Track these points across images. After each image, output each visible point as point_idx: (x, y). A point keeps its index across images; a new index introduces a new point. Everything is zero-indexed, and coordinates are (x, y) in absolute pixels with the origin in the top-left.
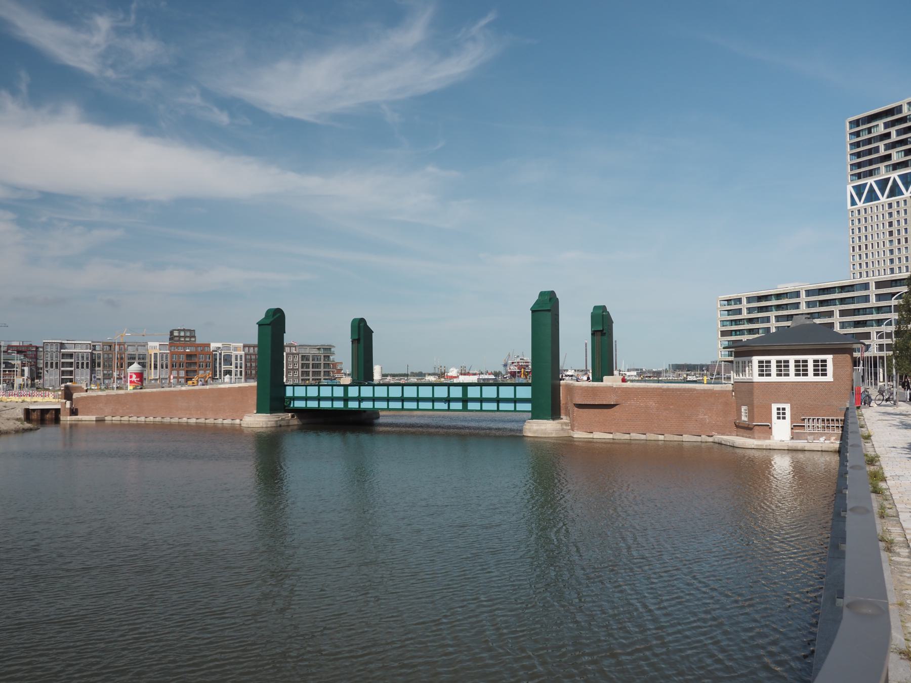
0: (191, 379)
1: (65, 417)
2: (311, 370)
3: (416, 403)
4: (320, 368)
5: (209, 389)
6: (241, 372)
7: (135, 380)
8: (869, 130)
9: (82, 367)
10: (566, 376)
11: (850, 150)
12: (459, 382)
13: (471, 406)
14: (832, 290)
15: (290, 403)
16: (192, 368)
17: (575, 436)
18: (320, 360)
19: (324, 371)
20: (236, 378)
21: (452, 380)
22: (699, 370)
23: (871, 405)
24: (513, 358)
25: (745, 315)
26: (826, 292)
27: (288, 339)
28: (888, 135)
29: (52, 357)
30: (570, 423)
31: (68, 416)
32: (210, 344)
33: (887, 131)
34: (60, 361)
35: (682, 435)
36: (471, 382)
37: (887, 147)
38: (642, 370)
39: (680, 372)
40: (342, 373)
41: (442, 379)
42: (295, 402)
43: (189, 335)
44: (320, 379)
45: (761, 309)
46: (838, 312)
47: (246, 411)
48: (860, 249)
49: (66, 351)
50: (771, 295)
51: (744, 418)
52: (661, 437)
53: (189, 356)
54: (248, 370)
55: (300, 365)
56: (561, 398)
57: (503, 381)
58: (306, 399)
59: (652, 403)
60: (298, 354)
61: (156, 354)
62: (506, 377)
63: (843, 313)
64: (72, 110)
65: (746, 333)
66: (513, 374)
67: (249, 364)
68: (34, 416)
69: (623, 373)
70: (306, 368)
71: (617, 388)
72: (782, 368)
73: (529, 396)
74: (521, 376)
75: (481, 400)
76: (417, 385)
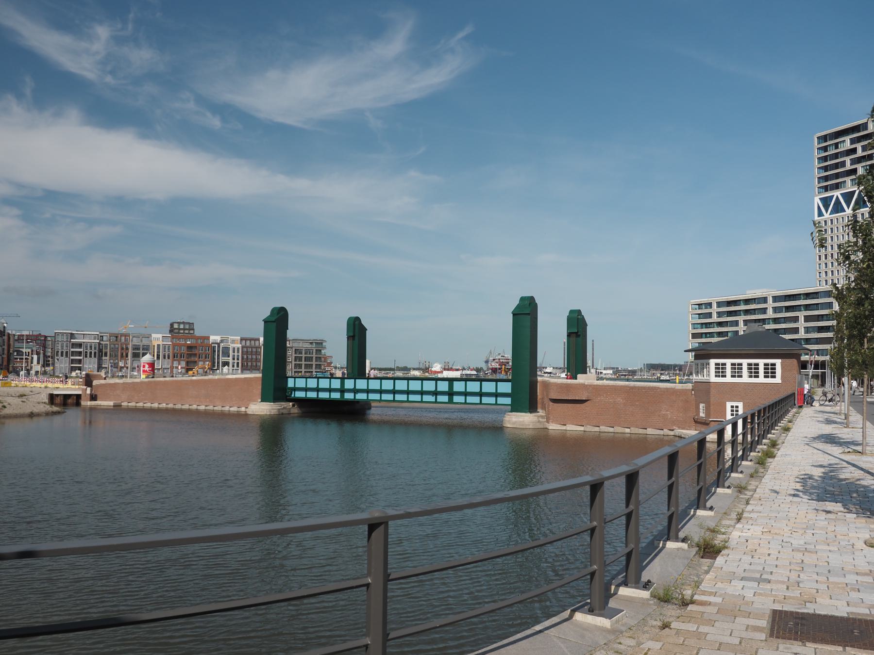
0: (191, 369)
1: (85, 402)
2: (303, 363)
3: (494, 398)
4: (312, 361)
5: (218, 379)
6: (238, 363)
7: (148, 369)
8: (836, 146)
9: (90, 356)
10: (545, 373)
11: (818, 164)
12: (443, 377)
13: (457, 399)
14: (797, 296)
15: (292, 393)
16: (193, 359)
17: (550, 428)
18: (312, 354)
19: (316, 364)
20: (233, 369)
21: (436, 375)
22: (672, 370)
23: (813, 405)
24: (495, 355)
25: (715, 318)
26: (792, 299)
27: (291, 334)
28: (854, 151)
29: (62, 347)
30: (546, 416)
31: (88, 401)
32: (209, 337)
33: (853, 146)
34: (70, 350)
35: (646, 429)
36: (455, 377)
37: (853, 162)
38: (618, 368)
39: (654, 372)
40: (332, 367)
41: (427, 374)
42: (296, 392)
43: (188, 328)
44: (312, 372)
45: (730, 314)
46: (803, 317)
47: (252, 400)
48: (826, 258)
49: (76, 341)
50: (740, 300)
51: (702, 415)
52: (627, 430)
53: (190, 348)
54: (245, 361)
55: (293, 358)
56: (538, 394)
57: (485, 377)
58: (306, 390)
59: (620, 400)
60: (292, 348)
61: (159, 345)
62: (488, 373)
63: (807, 319)
64: (74, 114)
65: (716, 336)
66: (494, 370)
67: (245, 357)
68: (58, 400)
69: (600, 371)
70: (299, 361)
71: (589, 385)
72: (737, 371)
73: (509, 391)
74: (501, 372)
75: (466, 394)
76: (422, 379)
